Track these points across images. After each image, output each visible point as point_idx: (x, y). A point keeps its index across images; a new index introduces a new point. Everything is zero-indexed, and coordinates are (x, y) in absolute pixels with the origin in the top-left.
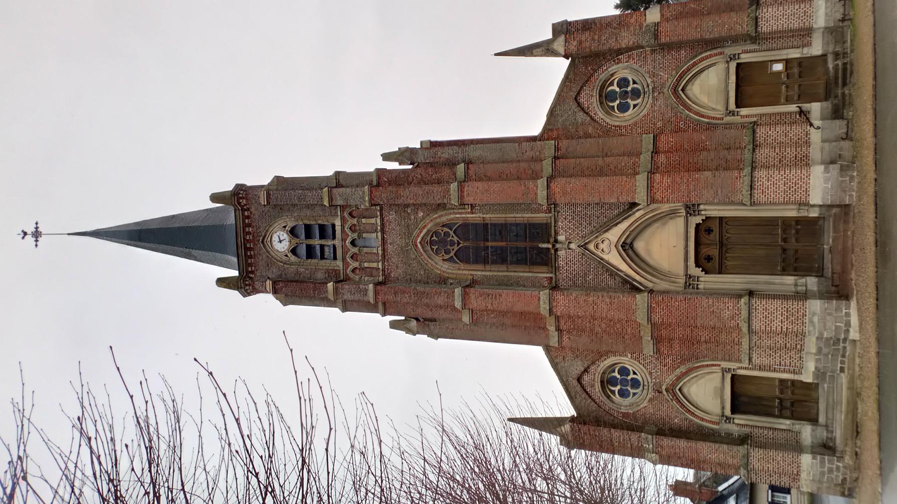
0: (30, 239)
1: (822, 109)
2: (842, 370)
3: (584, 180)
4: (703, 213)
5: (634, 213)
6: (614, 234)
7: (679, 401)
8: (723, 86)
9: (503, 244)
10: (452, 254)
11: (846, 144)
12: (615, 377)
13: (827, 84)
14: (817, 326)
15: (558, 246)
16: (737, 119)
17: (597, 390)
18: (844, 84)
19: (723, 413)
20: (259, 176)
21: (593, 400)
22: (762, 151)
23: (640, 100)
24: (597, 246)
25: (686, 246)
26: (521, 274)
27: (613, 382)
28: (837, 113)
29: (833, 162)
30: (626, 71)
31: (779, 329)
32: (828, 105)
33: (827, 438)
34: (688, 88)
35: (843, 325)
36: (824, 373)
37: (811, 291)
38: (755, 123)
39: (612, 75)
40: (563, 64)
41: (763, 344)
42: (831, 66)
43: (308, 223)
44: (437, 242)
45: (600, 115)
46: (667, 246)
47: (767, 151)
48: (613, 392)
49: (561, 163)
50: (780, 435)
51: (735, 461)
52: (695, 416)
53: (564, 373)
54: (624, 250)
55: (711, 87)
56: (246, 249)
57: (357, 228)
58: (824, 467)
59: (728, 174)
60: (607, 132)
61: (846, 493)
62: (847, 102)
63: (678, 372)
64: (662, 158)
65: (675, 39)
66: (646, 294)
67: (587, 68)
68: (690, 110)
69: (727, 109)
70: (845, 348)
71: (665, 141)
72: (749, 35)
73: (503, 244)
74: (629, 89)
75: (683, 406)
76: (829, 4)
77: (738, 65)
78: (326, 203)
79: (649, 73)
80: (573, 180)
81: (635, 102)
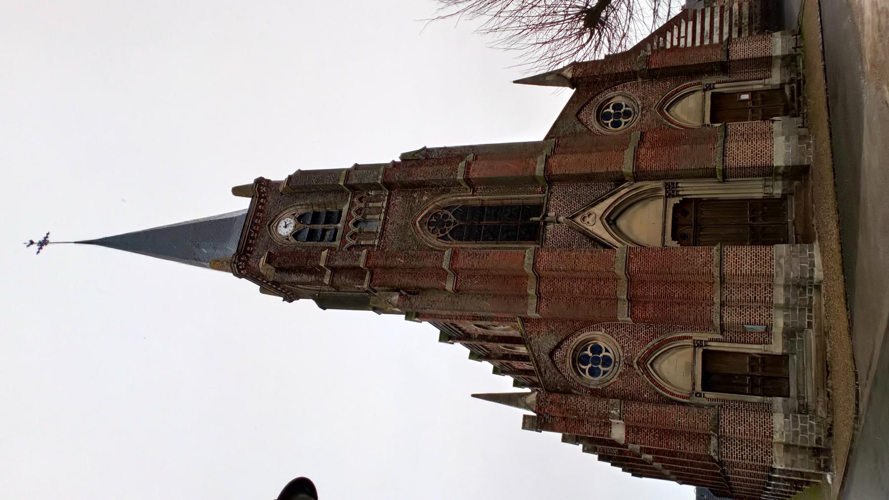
0: (35, 247)
2: (810, 324)
6: (599, 209)
7: (649, 376)
10: (447, 232)
23: (630, 119)
27: (585, 360)
31: (749, 272)
41: (734, 298)
42: (788, 92)
44: (436, 222)
45: (596, 126)
53: (537, 348)
58: (796, 426)
61: (822, 465)
67: (588, 93)
70: (811, 298)
75: (653, 380)
77: (713, 95)
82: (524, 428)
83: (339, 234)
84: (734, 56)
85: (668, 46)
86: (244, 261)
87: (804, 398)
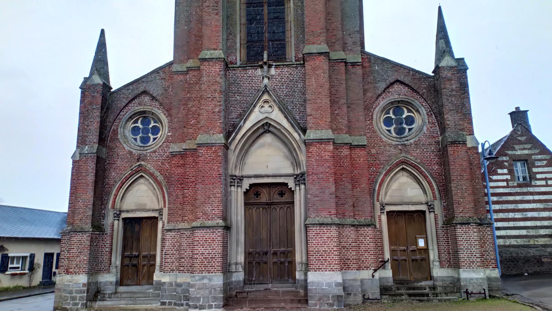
1: (387, 278)
2: (163, 304)
3: (327, 86)
4: (298, 188)
5: (297, 131)
6: (277, 116)
7: (131, 175)
8: (406, 200)
9: (266, 20)
11: (359, 299)
12: (150, 124)
13: (407, 282)
15: (265, 67)
16: (378, 212)
17: (135, 108)
18: (410, 295)
19: (124, 211)
21: (127, 105)
22: (352, 232)
23: (394, 134)
24: (266, 102)
25: (268, 176)
26: (238, 37)
27: (146, 122)
28: (384, 290)
29: (344, 288)
30: (421, 122)
31: (196, 252)
32: (391, 282)
33: (105, 294)
34: (405, 173)
35: (201, 303)
36: (160, 289)
37: (231, 277)
38: (375, 226)
39: (417, 111)
40: (428, 68)
42: (423, 283)
45: (382, 103)
46: (268, 161)
47: (352, 236)
48: (136, 122)
49: (342, 67)
50: (106, 258)
51: (77, 222)
52: (118, 191)
53: (150, 79)
54: (263, 125)
55: (405, 190)
59: (333, 205)
60: (368, 109)
62: (395, 298)
63: (157, 174)
64: (345, 152)
65: (451, 158)
66: (223, 141)
68: (386, 175)
69: (387, 204)
70: (182, 305)
71: (361, 156)
73: (266, 20)
74: (405, 126)
75: (127, 179)
77: (423, 212)
79: (419, 140)
80: (327, 76)
81: (392, 131)
85: (535, 170)
87: (110, 298)
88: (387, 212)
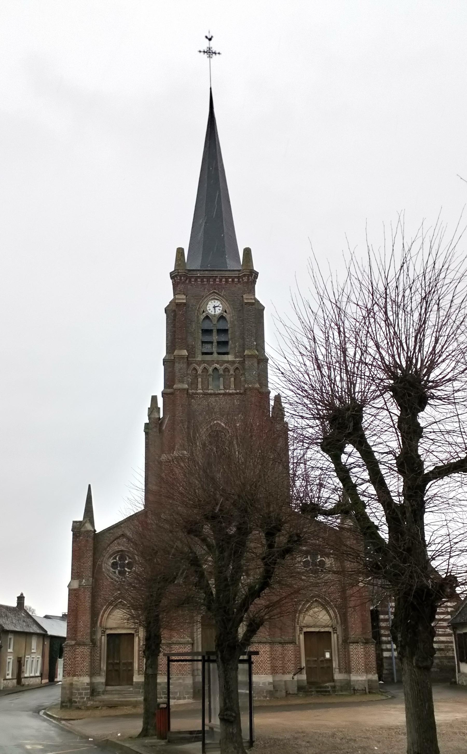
0: (205, 45)
11: (284, 693)
14: (177, 682)
18: (317, 692)
20: (262, 292)
22: (280, 648)
28: (300, 688)
29: (274, 687)
33: (99, 691)
38: (296, 643)
42: (327, 684)
43: (229, 332)
52: (104, 613)
56: (208, 278)
57: (227, 373)
61: (64, 704)
72: (348, 638)
76: (364, 682)
77: (330, 633)
78: (246, 352)
82: (74, 522)
83: (208, 358)
84: (352, 647)
86: (181, 279)
87: (103, 694)
88: (304, 632)
